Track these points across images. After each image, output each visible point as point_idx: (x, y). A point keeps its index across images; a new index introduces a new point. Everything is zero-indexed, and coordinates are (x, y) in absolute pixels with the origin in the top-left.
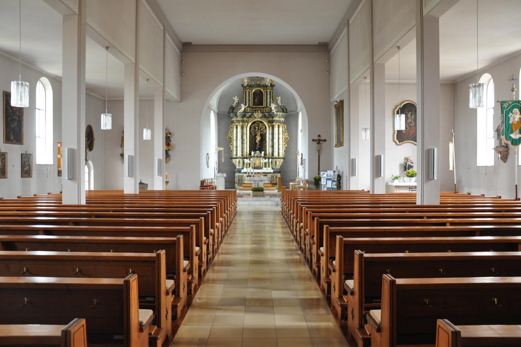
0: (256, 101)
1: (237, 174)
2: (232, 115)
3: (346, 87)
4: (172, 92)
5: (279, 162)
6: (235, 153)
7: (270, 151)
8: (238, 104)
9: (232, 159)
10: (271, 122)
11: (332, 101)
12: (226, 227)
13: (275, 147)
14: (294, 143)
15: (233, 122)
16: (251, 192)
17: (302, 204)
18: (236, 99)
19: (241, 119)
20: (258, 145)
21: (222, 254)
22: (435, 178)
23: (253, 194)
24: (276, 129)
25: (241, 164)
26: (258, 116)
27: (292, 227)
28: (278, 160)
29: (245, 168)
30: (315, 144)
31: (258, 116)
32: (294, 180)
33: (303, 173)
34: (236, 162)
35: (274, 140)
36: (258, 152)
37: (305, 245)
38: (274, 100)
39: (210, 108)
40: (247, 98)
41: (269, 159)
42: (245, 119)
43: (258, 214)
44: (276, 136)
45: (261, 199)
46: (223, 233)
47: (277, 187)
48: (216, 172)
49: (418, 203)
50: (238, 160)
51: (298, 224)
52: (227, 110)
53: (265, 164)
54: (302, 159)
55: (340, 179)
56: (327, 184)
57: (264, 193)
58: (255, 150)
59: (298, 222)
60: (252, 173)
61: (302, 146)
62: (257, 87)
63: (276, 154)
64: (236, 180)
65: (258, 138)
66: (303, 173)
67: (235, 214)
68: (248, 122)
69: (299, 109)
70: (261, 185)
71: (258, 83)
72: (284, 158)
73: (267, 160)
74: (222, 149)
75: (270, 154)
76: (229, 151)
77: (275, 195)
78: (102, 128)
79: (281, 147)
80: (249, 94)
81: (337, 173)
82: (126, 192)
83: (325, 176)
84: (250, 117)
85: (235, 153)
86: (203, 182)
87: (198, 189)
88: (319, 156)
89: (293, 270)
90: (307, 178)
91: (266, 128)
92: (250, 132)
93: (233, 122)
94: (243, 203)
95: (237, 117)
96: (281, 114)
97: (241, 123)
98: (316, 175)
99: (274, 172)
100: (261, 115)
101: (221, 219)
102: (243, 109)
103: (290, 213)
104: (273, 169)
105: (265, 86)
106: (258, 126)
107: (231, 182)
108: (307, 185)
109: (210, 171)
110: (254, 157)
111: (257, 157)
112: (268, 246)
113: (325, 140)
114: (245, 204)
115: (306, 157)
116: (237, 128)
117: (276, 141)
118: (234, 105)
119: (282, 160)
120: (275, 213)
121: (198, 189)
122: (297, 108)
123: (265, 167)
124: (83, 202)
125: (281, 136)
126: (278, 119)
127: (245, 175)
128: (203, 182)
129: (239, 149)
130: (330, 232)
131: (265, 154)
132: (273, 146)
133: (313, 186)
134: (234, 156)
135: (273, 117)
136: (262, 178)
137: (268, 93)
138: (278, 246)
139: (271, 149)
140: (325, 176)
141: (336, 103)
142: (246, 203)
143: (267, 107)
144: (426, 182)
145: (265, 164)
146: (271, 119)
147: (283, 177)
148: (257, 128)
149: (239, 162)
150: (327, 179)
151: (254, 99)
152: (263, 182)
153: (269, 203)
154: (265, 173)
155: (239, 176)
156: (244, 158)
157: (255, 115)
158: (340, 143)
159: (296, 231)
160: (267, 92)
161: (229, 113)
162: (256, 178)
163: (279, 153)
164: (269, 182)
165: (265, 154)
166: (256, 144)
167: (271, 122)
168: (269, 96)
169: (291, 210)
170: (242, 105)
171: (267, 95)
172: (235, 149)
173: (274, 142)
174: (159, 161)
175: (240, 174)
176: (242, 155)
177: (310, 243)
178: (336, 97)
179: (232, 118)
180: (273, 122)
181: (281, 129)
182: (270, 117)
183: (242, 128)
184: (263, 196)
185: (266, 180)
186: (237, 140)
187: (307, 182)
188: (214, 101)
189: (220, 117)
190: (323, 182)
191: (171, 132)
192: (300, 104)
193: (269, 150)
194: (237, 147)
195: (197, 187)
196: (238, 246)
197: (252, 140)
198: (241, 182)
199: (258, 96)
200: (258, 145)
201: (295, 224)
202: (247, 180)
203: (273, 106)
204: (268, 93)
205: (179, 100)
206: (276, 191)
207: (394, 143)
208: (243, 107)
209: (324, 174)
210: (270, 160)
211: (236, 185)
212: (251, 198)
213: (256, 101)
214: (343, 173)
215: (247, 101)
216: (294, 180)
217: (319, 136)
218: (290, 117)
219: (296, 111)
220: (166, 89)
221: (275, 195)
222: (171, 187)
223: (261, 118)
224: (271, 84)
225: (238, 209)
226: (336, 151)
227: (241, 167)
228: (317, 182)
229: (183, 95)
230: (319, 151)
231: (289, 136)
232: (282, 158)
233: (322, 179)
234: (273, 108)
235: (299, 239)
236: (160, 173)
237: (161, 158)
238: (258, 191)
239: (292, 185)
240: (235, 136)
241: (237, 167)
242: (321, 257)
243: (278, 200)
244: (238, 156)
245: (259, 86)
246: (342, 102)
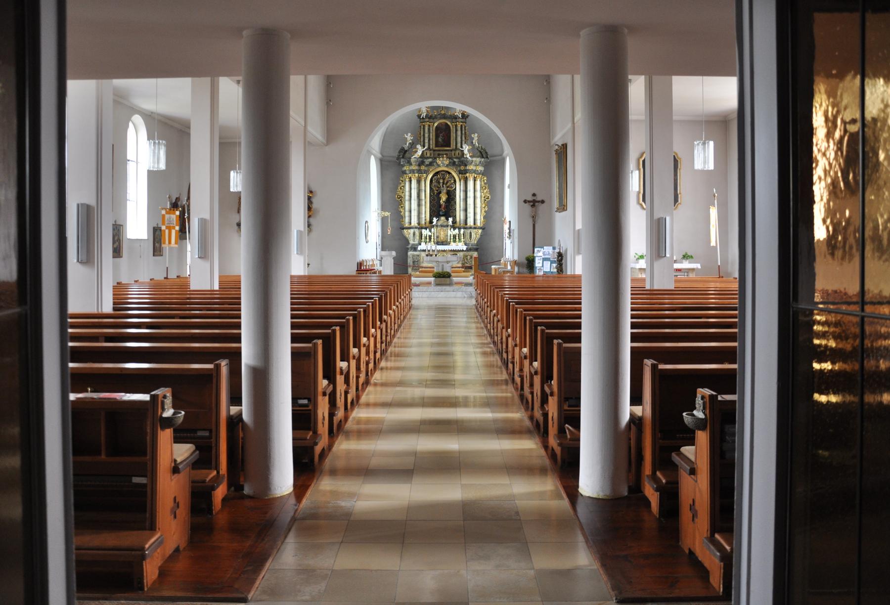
0: (440, 140)
1: (410, 253)
2: (402, 161)
3: (570, 125)
4: (316, 132)
5: (476, 235)
6: (407, 220)
7: (462, 218)
8: (413, 145)
9: (403, 229)
10: (463, 172)
11: (553, 142)
12: (384, 345)
13: (468, 210)
14: (496, 204)
15: (404, 172)
16: (433, 279)
17: (517, 303)
18: (409, 138)
19: (416, 168)
20: (443, 208)
21: (368, 405)
22: (668, 255)
23: (435, 281)
24: (471, 184)
25: (417, 237)
26: (443, 164)
27: (505, 355)
28: (473, 232)
29: (423, 244)
30: (527, 206)
31: (443, 164)
32: (498, 262)
33: (510, 251)
34: (409, 233)
35: (468, 199)
36: (443, 218)
37: (532, 393)
38: (467, 139)
39: (369, 153)
40: (427, 135)
41: (460, 229)
42: (423, 168)
43: (443, 311)
44: (470, 194)
45: (448, 288)
46: (378, 355)
47: (473, 272)
48: (379, 250)
49: (648, 287)
50: (412, 231)
51: (517, 350)
52: (396, 154)
53: (455, 236)
54: (509, 229)
55: (561, 260)
56: (544, 266)
57: (451, 281)
58: (438, 216)
59: (516, 345)
60: (433, 251)
61: (510, 210)
62: (441, 118)
63: (470, 222)
64: (410, 261)
65: (444, 197)
66: (510, 251)
67: (410, 308)
68: (427, 172)
69: (505, 153)
70: (448, 269)
71: (443, 112)
72: (483, 228)
73: (457, 231)
74: (387, 214)
75: (462, 222)
76: (398, 216)
77: (468, 284)
78: (232, 190)
79: (478, 210)
80: (429, 129)
81: (557, 250)
82: (194, 286)
83: (541, 254)
84: (431, 164)
85: (407, 220)
86: (360, 264)
87: (354, 273)
88: (534, 225)
89: (494, 393)
90: (516, 258)
91: (455, 181)
92: (431, 188)
93: (404, 172)
94: (421, 294)
95: (411, 164)
96: (478, 160)
97: (417, 175)
98: (530, 254)
99: (468, 250)
100: (447, 162)
101: (394, 307)
102: (420, 153)
103: (492, 314)
104: (466, 244)
105: (456, 117)
106: (444, 179)
107: (401, 265)
108: (516, 269)
109: (370, 248)
110: (437, 226)
111: (442, 226)
112: (458, 376)
113: (543, 202)
114: (424, 296)
115: (514, 226)
116: (410, 181)
117: (470, 201)
118: (406, 147)
119: (480, 231)
120: (467, 308)
121: (354, 273)
122: (503, 151)
123: (455, 241)
124: (216, 287)
125: (478, 194)
126: (474, 168)
127: (423, 254)
128: (360, 264)
129: (414, 214)
130: (547, 338)
131: (454, 222)
132: (466, 210)
133: (525, 270)
134: (407, 225)
135: (466, 165)
136: (449, 256)
137: (459, 128)
138: (471, 355)
139: (462, 214)
140: (541, 254)
141: (557, 147)
142: (425, 295)
143: (456, 148)
144: (656, 259)
145: (455, 236)
146: (462, 168)
147: (481, 256)
148: (441, 181)
149: (414, 234)
150: (544, 259)
151: (437, 136)
152: (450, 264)
153: (459, 294)
154: (454, 251)
155: (413, 256)
156: (422, 228)
157: (439, 161)
158: (563, 207)
159: (513, 363)
160: (456, 126)
161: (398, 158)
162: (440, 258)
163: (475, 220)
164: (460, 265)
165: (454, 222)
166: (440, 206)
167: (463, 172)
168: (459, 133)
169: (508, 327)
170: (419, 147)
171: (456, 130)
172: (407, 214)
173: (468, 202)
174: (300, 233)
175: (415, 253)
176: (419, 224)
177: (530, 372)
178: (558, 139)
179: (403, 166)
180: (466, 172)
181: (478, 182)
182: (461, 164)
183: (419, 182)
184: (450, 284)
185: (455, 262)
186: (410, 200)
187: (515, 263)
188: (375, 142)
189: (384, 164)
190: (538, 263)
191: (313, 190)
192: (507, 150)
193: (460, 215)
194: (410, 211)
195: (352, 270)
196: (417, 338)
197: (434, 200)
198: (417, 266)
199: (443, 134)
200: (443, 208)
201: (510, 348)
202: (426, 262)
203: (466, 149)
204: (459, 128)
205: (325, 142)
206: (471, 279)
207: (639, 207)
208: (420, 150)
209: (539, 251)
210: (462, 231)
211: (410, 270)
212: (432, 288)
213: (440, 140)
214: (566, 251)
215: (427, 141)
216: (498, 262)
217: (534, 195)
218: (491, 163)
219: (501, 155)
220: (309, 128)
221: (468, 284)
222: (315, 271)
223: (447, 166)
224: (463, 115)
225: (413, 302)
226: (559, 217)
227: (416, 242)
228: (530, 263)
229: (331, 135)
230: (534, 218)
231: (490, 194)
232: (481, 228)
233: (537, 259)
234: (466, 152)
235: (518, 380)
236: (300, 251)
237: (302, 229)
238: (443, 277)
239: (495, 270)
240: (407, 194)
241: (411, 242)
242: (550, 398)
243: (471, 289)
244: (413, 224)
245: (444, 117)
246: (565, 146)
